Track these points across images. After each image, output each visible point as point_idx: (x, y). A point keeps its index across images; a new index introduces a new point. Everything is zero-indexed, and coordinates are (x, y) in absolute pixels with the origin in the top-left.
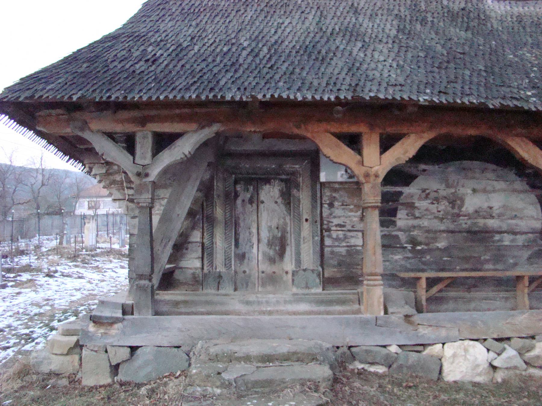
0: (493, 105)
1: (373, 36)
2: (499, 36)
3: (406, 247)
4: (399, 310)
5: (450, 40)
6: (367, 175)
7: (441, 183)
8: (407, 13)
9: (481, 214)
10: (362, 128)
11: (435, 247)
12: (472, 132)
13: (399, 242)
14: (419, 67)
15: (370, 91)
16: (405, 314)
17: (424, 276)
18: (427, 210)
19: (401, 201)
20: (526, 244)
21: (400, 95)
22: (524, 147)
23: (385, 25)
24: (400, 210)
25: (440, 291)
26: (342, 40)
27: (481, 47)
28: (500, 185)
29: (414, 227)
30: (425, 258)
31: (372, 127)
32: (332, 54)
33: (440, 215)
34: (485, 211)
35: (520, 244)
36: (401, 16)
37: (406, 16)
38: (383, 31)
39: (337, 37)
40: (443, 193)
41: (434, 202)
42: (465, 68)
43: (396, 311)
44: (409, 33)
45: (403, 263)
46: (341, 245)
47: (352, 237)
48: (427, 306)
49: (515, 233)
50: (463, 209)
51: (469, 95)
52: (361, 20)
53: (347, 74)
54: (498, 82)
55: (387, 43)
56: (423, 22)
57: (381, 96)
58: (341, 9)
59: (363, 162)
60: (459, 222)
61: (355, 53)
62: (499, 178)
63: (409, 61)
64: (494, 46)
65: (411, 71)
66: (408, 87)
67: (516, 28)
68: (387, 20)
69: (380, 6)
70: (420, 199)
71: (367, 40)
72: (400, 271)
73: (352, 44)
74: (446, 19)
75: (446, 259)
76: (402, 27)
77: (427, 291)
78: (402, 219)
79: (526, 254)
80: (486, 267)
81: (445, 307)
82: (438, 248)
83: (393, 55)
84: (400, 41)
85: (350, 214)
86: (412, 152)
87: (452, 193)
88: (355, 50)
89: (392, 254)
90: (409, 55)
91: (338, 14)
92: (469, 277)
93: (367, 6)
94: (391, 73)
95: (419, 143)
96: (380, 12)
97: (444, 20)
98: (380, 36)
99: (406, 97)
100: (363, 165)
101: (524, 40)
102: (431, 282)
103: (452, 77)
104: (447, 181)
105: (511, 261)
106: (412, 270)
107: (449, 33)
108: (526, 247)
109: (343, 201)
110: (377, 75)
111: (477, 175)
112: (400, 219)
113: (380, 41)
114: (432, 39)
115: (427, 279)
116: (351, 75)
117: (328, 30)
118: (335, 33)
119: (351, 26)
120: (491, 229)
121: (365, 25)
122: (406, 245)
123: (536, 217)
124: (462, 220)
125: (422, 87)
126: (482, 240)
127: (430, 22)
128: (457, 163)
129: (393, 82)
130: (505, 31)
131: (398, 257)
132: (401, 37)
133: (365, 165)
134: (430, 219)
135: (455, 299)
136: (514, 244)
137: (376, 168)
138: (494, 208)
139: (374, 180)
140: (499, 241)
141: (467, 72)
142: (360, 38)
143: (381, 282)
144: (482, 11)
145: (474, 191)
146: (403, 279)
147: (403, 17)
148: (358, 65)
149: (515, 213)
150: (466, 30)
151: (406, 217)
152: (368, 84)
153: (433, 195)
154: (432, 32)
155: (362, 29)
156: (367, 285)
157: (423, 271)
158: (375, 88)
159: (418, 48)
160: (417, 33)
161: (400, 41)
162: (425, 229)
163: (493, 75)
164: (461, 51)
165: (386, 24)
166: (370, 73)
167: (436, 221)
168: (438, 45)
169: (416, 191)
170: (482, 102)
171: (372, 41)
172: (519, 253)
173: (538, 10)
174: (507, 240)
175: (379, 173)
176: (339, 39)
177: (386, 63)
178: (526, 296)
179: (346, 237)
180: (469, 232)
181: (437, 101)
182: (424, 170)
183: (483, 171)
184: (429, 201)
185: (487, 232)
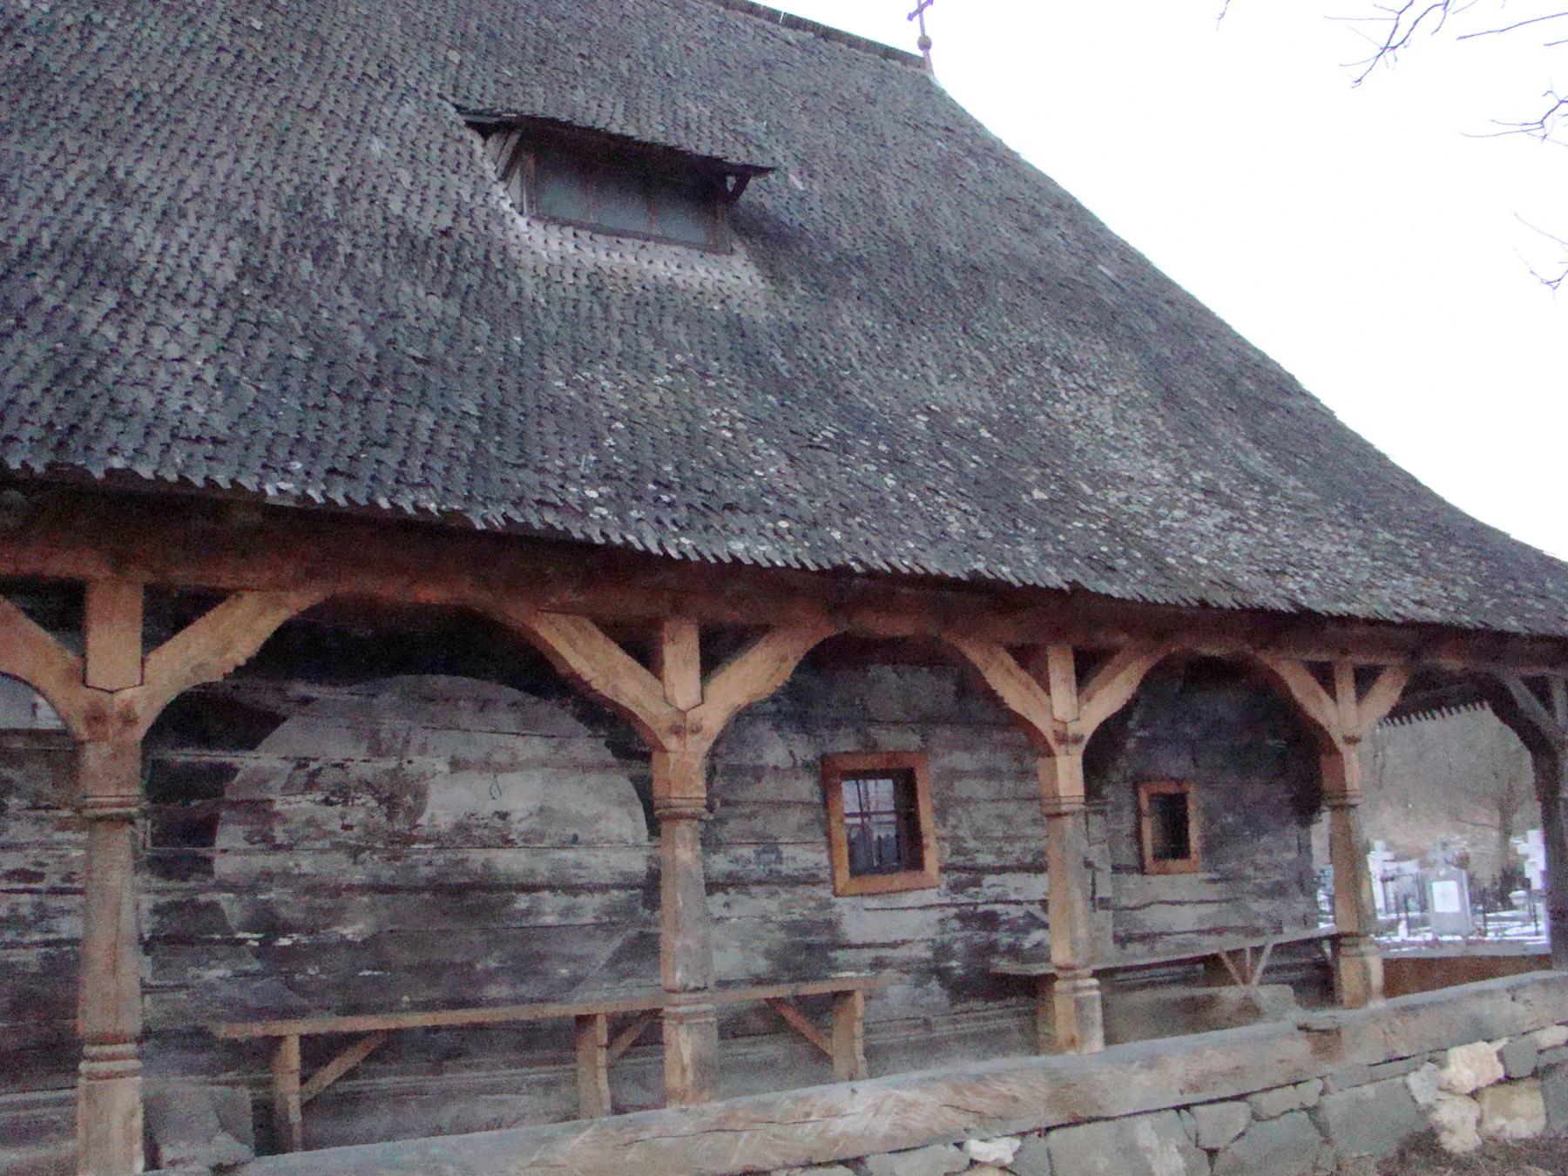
0: (485, 521)
1: (161, 278)
2: (536, 320)
3: (245, 940)
4: (200, 1150)
5: (394, 316)
6: (96, 718)
7: (358, 739)
8: (278, 221)
9: (476, 833)
10: (86, 565)
11: (334, 939)
12: (433, 594)
13: (225, 929)
14: (284, 389)
15: (112, 451)
16: (214, 1162)
17: (294, 1030)
18: (310, 822)
19: (228, 796)
20: (605, 919)
21: (206, 471)
22: (580, 643)
23: (204, 249)
24: (226, 822)
25: (351, 1074)
26: (57, 277)
27: (479, 349)
28: (536, 747)
29: (268, 876)
30: (304, 972)
31: (120, 562)
32: (12, 321)
33: (351, 838)
34: (486, 826)
35: (589, 919)
36: (257, 229)
37: (273, 229)
38: (193, 267)
39: (41, 267)
40: (363, 769)
41: (334, 799)
42: (422, 403)
43: (184, 1154)
44: (275, 284)
45: (227, 991)
46: (26, 940)
47: (63, 912)
48: (304, 1124)
49: (572, 889)
50: (422, 820)
51: (418, 485)
52: (128, 223)
53: (47, 390)
54: (511, 456)
55: (199, 304)
56: (323, 253)
57: (145, 471)
58: (70, 178)
59: (85, 675)
60: (409, 861)
61: (87, 328)
62: (529, 726)
63: (256, 367)
64: (516, 349)
65: (256, 401)
66: (238, 447)
67: (584, 308)
68: (212, 234)
69: (196, 189)
70: (288, 788)
71: (137, 289)
72: (216, 1017)
73: (84, 294)
74: (391, 253)
75: (367, 973)
76: (255, 261)
77: (304, 1080)
78: (232, 854)
79: (603, 950)
80: (493, 991)
81: (364, 1124)
82: (350, 945)
83: (210, 344)
84: (242, 304)
85: (58, 836)
86: (245, 648)
87: (386, 772)
88: (93, 316)
89: (198, 964)
90: (262, 350)
91: (59, 193)
92: (436, 1029)
93: (157, 181)
94: (192, 401)
95: (268, 624)
96: (191, 208)
97: (385, 257)
98: (181, 283)
99: (222, 480)
100: (84, 682)
101: (602, 344)
102: (318, 1051)
103: (380, 427)
104: (375, 734)
105: (564, 972)
106: (259, 1014)
107: (396, 298)
108: (605, 927)
109: (39, 795)
110: (148, 401)
111: (465, 719)
112: (224, 851)
113: (179, 295)
114: (340, 308)
115: (305, 1040)
116: (61, 394)
117: (14, 242)
118: (35, 251)
119: (93, 237)
120: (502, 880)
121: (139, 242)
122: (240, 935)
123: (631, 841)
124: (419, 851)
125: (281, 453)
126: (473, 914)
127: (342, 258)
128: (408, 679)
129: (194, 428)
130: (555, 310)
131: (214, 974)
132: (246, 292)
133: (92, 678)
134: (322, 851)
135: (398, 1098)
136: (572, 920)
137: (127, 694)
138: (514, 817)
139: (120, 733)
140: (528, 913)
141: (427, 419)
142: (115, 278)
143: (135, 1064)
144: (497, 246)
145: (456, 765)
146: (233, 1045)
147: (264, 231)
148: (92, 364)
149: (571, 831)
150: (445, 296)
151: (245, 845)
152: (113, 427)
153: (330, 777)
154: (345, 290)
155: (130, 254)
156: (91, 1076)
157: (286, 1013)
158: (129, 446)
159: (293, 330)
160: (300, 285)
161: (242, 304)
162: (302, 881)
163: (500, 434)
164: (419, 355)
165: (207, 247)
166: (126, 395)
167: (340, 856)
168: (354, 327)
169: (279, 764)
170: (454, 511)
171: (152, 295)
172: (588, 948)
173: (646, 266)
174: (550, 909)
175: (138, 709)
176: (45, 275)
177: (184, 367)
178: (603, 1075)
179: (42, 914)
180: (437, 886)
181: (319, 499)
182: (306, 701)
183: (484, 705)
184: (319, 796)
185: (489, 888)
